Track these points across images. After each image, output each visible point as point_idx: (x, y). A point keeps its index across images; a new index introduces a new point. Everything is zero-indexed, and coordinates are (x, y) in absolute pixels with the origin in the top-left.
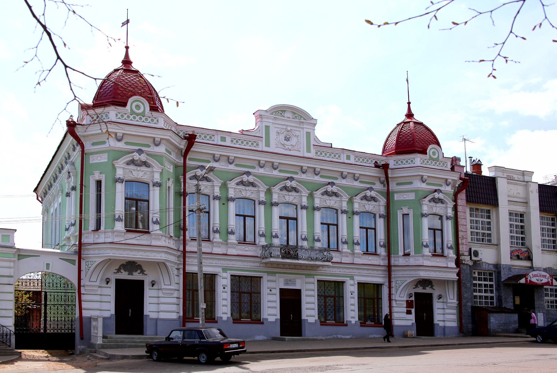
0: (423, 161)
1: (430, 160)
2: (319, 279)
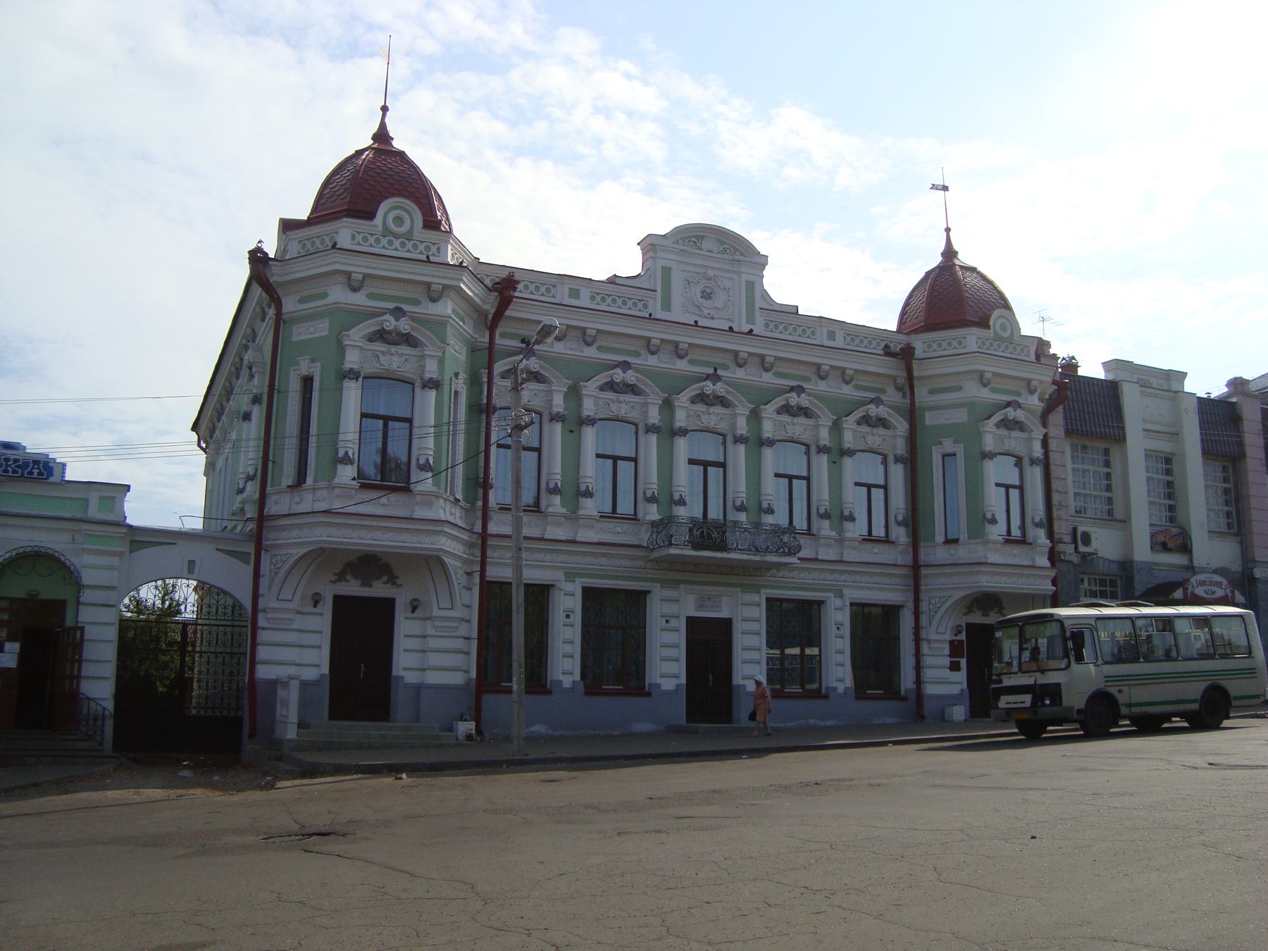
0: (983, 343)
1: (995, 341)
2: (587, 585)
